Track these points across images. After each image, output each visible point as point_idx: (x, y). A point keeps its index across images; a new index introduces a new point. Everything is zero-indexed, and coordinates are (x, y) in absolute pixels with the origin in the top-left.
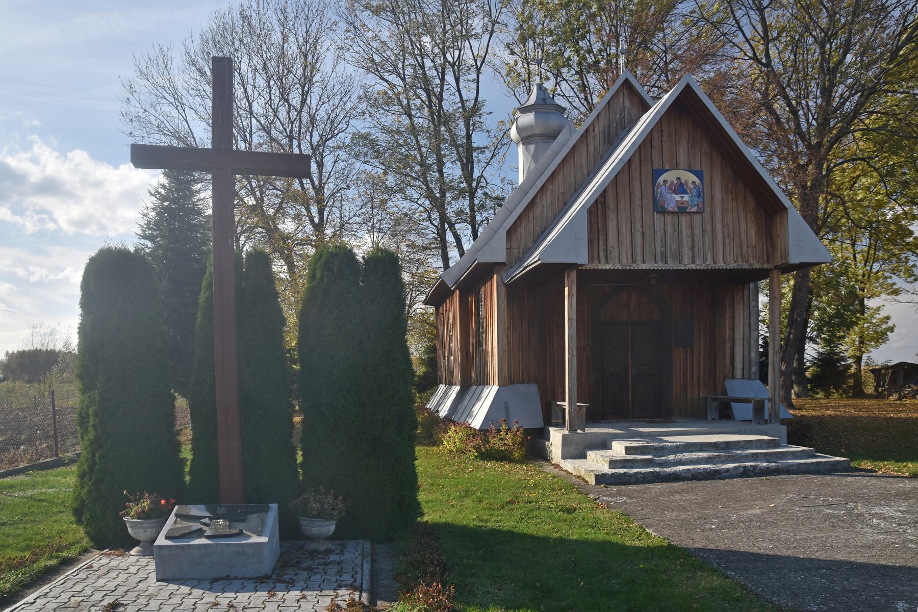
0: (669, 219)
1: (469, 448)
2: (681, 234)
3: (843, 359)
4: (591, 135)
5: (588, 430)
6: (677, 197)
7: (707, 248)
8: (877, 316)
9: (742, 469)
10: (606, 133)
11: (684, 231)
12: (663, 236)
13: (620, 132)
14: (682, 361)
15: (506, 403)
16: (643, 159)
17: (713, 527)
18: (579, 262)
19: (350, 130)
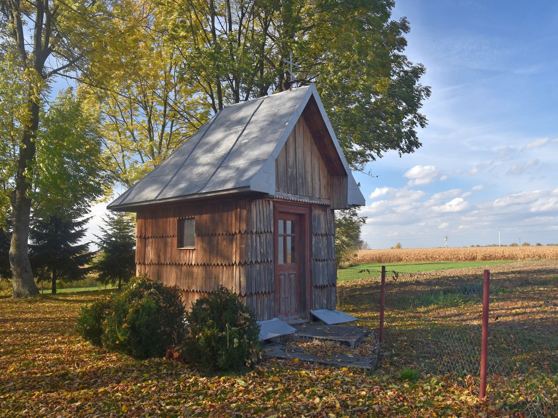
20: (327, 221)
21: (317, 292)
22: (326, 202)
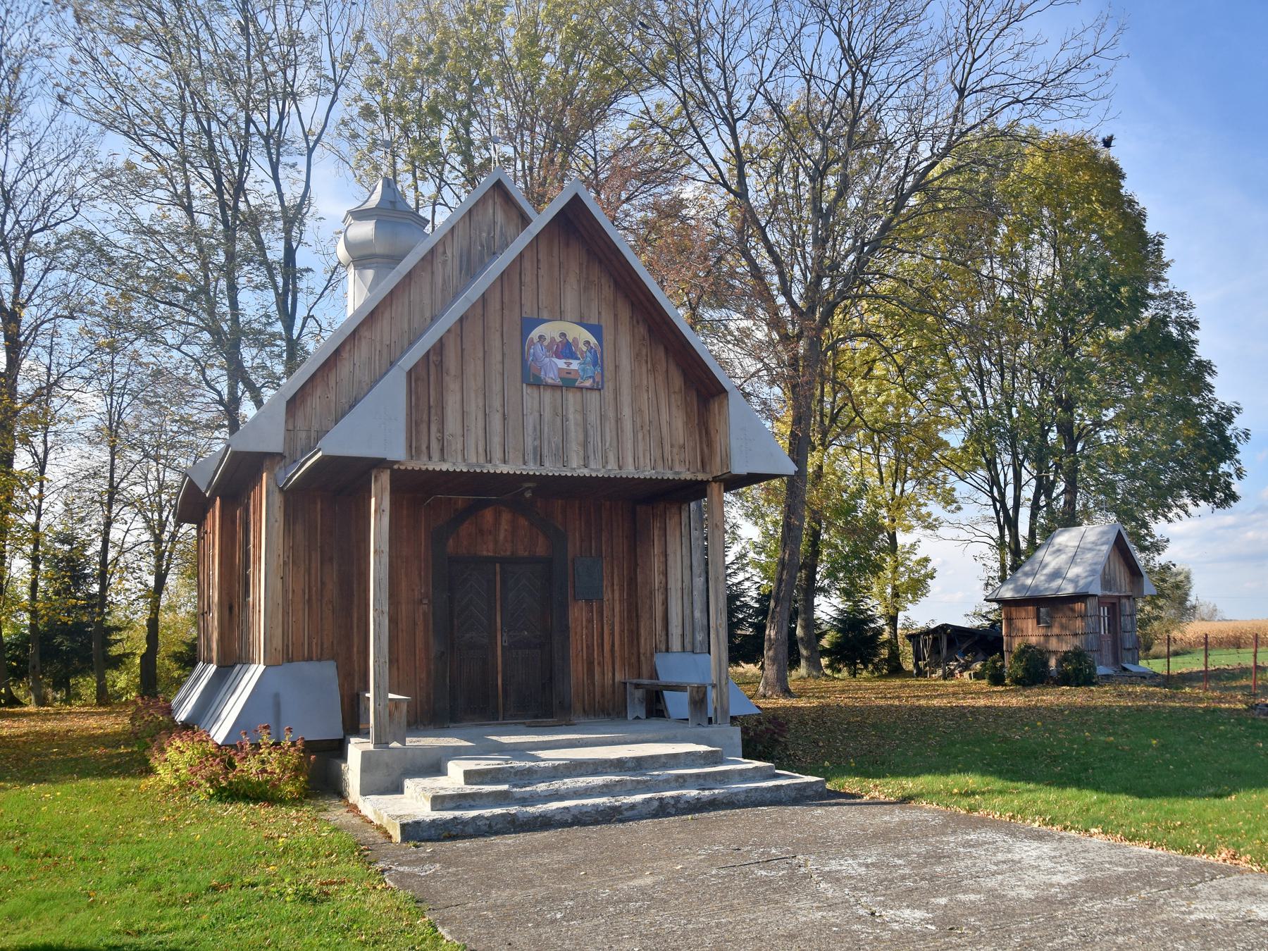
0: (547, 396)
1: (198, 779)
2: (567, 420)
3: (873, 620)
4: (439, 260)
5: (411, 742)
6: (561, 363)
7: (608, 444)
8: (914, 558)
9: (656, 804)
10: (465, 258)
11: (571, 417)
12: (538, 422)
13: (487, 260)
14: (584, 623)
15: (277, 697)
16: (506, 300)
17: (559, 916)
18: (391, 457)
19: (76, 222)
20: (1130, 606)
21: (1125, 652)
22: (1130, 594)
